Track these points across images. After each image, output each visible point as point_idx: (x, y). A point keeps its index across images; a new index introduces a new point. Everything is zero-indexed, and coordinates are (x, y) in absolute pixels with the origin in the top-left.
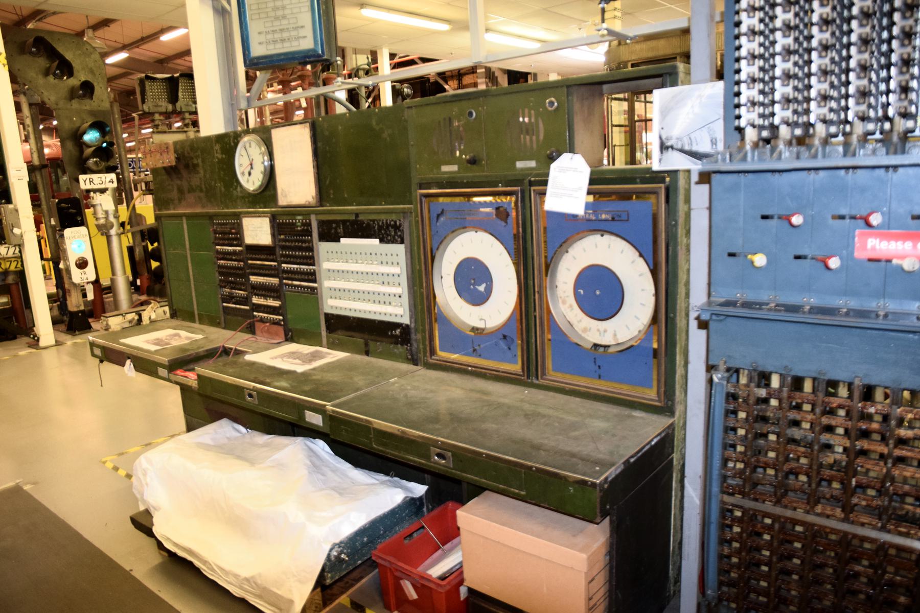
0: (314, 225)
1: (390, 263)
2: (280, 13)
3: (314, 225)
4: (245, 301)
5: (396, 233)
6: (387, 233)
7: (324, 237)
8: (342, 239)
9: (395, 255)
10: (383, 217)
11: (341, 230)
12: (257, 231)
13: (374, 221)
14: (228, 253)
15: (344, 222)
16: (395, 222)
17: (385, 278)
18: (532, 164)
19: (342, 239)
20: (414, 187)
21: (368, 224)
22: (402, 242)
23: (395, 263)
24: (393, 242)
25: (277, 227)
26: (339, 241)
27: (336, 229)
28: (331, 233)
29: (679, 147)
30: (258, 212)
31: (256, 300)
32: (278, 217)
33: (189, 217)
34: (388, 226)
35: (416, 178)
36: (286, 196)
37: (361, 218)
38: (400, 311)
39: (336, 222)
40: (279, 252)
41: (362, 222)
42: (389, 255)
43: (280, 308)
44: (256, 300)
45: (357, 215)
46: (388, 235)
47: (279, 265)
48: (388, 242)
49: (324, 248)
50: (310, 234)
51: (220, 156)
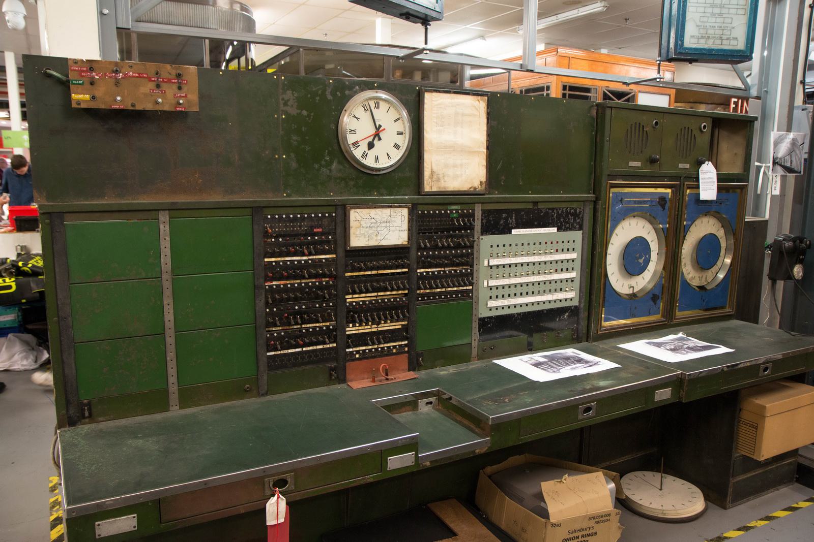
0: (478, 214)
1: (560, 250)
2: (717, 10)
3: (478, 214)
4: (331, 335)
5: (575, 220)
6: (564, 220)
7: (488, 229)
8: (513, 231)
9: (571, 242)
10: (564, 205)
11: (512, 221)
12: (380, 227)
13: (553, 209)
14: (300, 266)
15: (518, 211)
16: (576, 210)
17: (560, 266)
18: (687, 166)
19: (513, 231)
20: (604, 178)
21: (547, 213)
22: (580, 228)
23: (571, 249)
24: (571, 230)
25: (420, 224)
26: (510, 233)
27: (506, 219)
28: (498, 224)
29: (780, 163)
30: (384, 201)
31: (351, 330)
32: (420, 207)
33: (173, 209)
34: (568, 214)
35: (606, 172)
36: (438, 180)
37: (540, 206)
38: (571, 295)
39: (509, 212)
40: (413, 253)
41: (540, 211)
42: (566, 242)
43: (405, 328)
44: (351, 330)
45: (535, 203)
46: (566, 223)
47: (412, 271)
48: (567, 229)
49: (486, 242)
50: (472, 228)
51: (294, 111)
